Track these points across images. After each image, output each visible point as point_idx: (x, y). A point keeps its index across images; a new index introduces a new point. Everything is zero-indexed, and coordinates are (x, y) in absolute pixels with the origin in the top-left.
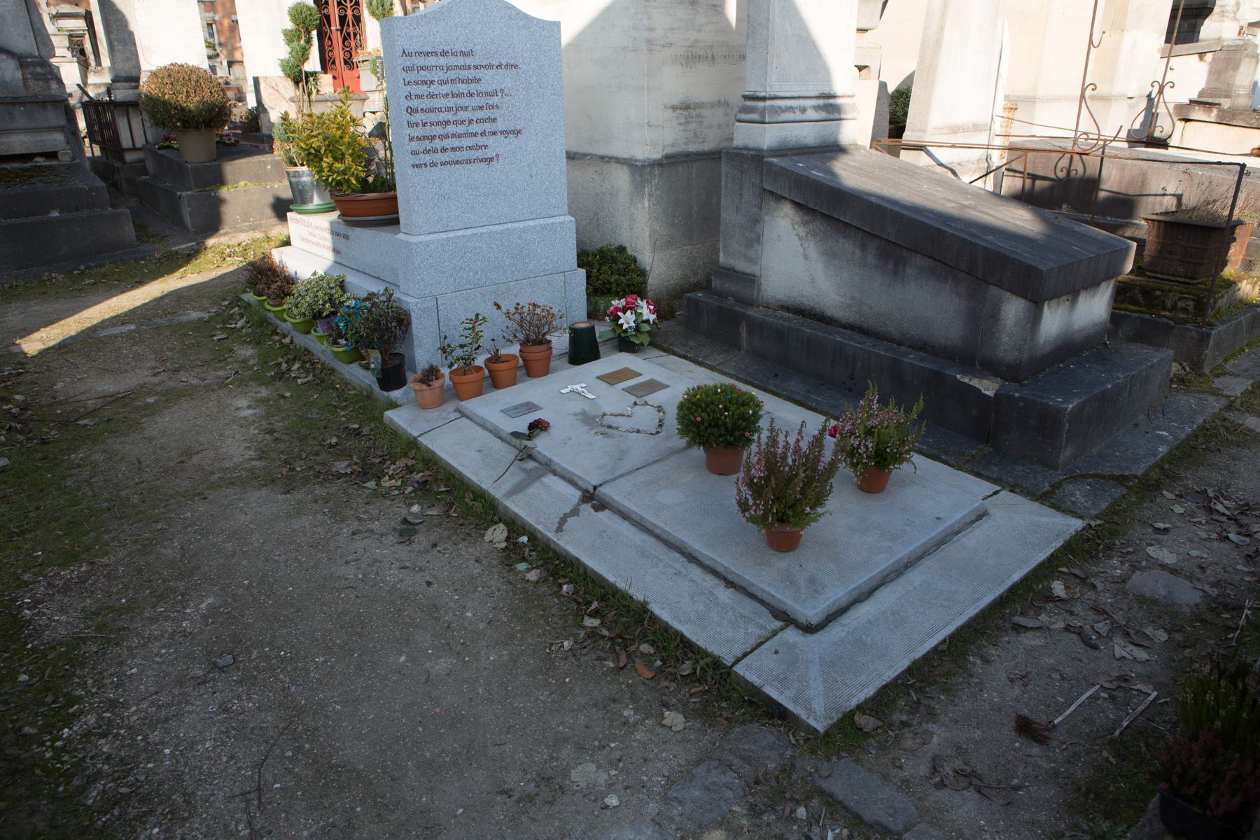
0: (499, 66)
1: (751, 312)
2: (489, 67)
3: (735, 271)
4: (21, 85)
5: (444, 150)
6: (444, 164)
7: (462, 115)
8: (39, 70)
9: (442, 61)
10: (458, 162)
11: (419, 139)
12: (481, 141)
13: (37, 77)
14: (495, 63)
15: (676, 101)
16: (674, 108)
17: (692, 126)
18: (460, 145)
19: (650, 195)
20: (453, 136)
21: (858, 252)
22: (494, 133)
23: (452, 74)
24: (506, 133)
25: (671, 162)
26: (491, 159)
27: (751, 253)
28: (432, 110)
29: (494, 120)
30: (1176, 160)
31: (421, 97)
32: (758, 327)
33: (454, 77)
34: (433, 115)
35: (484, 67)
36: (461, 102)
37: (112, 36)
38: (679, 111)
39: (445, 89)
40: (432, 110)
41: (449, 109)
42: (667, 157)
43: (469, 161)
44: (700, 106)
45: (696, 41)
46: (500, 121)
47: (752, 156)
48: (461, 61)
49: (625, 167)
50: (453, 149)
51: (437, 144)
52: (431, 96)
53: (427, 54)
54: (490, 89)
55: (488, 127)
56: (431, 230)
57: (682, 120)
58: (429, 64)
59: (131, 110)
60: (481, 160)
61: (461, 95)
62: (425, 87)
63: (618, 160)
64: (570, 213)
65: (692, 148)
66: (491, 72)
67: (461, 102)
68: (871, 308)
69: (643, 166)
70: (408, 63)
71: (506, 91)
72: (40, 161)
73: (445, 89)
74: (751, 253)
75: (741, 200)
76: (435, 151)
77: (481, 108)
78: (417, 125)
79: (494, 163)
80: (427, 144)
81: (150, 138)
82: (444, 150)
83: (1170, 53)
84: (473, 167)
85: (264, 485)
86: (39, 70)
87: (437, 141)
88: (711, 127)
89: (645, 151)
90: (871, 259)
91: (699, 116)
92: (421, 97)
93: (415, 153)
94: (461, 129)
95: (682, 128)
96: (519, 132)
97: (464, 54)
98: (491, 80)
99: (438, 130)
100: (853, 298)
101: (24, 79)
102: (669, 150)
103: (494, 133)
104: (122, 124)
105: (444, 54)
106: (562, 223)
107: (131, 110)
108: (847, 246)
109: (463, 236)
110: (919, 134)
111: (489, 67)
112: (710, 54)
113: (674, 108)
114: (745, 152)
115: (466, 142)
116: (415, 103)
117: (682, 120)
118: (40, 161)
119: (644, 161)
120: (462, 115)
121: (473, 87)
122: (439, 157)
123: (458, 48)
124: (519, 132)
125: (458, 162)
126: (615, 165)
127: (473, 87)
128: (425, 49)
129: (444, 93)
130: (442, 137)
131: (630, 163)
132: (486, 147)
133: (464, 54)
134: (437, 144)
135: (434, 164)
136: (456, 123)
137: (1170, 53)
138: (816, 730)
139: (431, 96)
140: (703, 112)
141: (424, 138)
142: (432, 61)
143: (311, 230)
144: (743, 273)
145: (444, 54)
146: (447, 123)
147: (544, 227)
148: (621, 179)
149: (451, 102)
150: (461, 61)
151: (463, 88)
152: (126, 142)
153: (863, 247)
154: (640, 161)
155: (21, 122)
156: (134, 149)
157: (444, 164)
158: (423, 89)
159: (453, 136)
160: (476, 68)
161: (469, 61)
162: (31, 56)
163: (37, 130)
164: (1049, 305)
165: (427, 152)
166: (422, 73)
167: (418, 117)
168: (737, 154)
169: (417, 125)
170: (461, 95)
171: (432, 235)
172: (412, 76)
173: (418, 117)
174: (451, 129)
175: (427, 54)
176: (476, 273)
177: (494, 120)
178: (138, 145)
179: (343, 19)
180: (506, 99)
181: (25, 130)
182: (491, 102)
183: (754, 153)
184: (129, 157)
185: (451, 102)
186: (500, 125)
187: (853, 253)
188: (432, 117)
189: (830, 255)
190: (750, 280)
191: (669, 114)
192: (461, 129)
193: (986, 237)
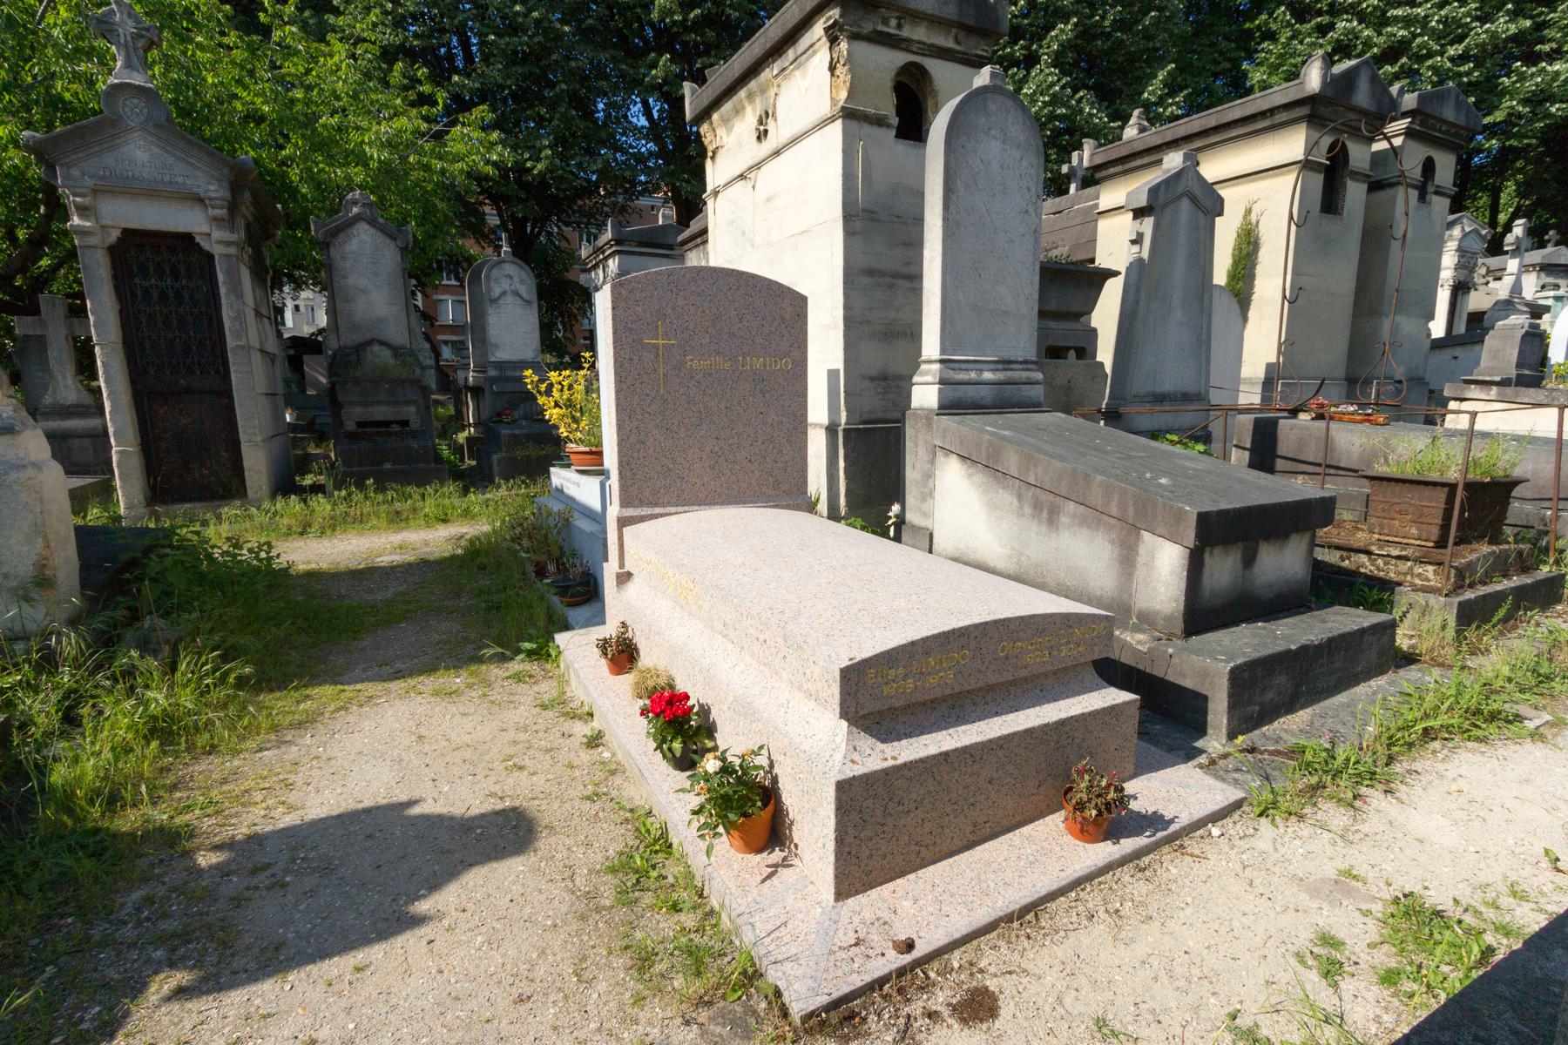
21: (1015, 502)
27: (925, 507)
57: (881, 390)
68: (1029, 558)
74: (925, 507)
83: (1321, 384)
85: (1315, 789)
90: (1028, 510)
91: (898, 387)
100: (1013, 549)
108: (1007, 498)
112: (908, 331)
113: (872, 379)
117: (881, 390)
118: (396, 428)
137: (1321, 384)
138: (1395, 641)
153: (1020, 497)
162: (404, 348)
164: (1211, 554)
189: (993, 506)
193: (1108, 368)
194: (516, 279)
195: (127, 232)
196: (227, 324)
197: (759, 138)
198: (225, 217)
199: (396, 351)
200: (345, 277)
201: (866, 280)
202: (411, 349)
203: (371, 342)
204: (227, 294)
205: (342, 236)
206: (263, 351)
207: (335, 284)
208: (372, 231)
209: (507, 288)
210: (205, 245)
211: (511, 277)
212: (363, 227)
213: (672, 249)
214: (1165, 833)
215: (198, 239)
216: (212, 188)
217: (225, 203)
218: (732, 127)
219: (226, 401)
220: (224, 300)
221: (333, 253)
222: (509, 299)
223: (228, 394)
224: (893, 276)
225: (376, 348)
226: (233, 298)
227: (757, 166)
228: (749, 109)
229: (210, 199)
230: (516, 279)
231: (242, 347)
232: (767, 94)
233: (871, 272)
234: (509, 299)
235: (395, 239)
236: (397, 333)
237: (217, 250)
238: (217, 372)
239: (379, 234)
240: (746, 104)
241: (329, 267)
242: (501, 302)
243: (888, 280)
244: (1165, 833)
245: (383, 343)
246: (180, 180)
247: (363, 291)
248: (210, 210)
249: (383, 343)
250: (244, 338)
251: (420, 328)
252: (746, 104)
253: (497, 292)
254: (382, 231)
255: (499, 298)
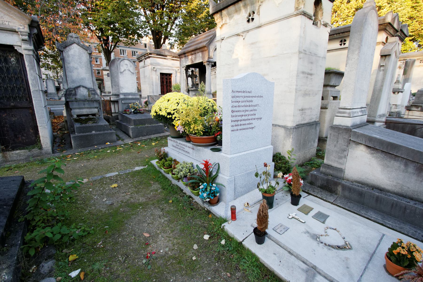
0: (258, 97)
1: (343, 182)
2: (255, 97)
3: (332, 166)
4: (88, 95)
5: (241, 125)
6: (240, 130)
7: (247, 113)
8: (93, 92)
9: (243, 94)
10: (244, 129)
11: (234, 121)
12: (251, 121)
13: (92, 94)
14: (257, 95)
15: (300, 108)
16: (300, 110)
17: (303, 116)
18: (245, 123)
19: (292, 138)
20: (244, 120)
22: (255, 119)
23: (245, 99)
24: (258, 119)
25: (298, 127)
26: (253, 128)
28: (239, 111)
29: (255, 115)
30: (400, 122)
31: (236, 107)
32: (344, 187)
33: (246, 100)
34: (239, 113)
35: (254, 97)
36: (247, 108)
37: (113, 84)
38: (301, 111)
39: (243, 104)
40: (239, 111)
41: (243, 111)
42: (297, 125)
43: (247, 129)
44: (305, 109)
45: (307, 89)
46: (256, 115)
47: (344, 128)
48: (248, 94)
49: (282, 128)
50: (243, 125)
51: (239, 123)
52: (239, 106)
53: (239, 92)
54: (255, 104)
55: (253, 117)
56: (235, 153)
58: (239, 95)
59: (115, 103)
60: (250, 128)
61: (247, 106)
62: (238, 103)
63: (279, 126)
64: (272, 145)
65: (303, 122)
66: (256, 98)
67: (247, 108)
69: (291, 129)
70: (233, 95)
71: (259, 105)
72: (91, 117)
73: (243, 104)
75: (337, 143)
76: (238, 125)
77: (252, 110)
78: (234, 116)
79: (254, 129)
80: (236, 123)
81: (120, 110)
82: (241, 125)
84: (248, 130)
86: (93, 92)
87: (239, 122)
88: (307, 116)
89: (290, 124)
92: (236, 107)
93: (232, 126)
94: (246, 118)
95: (301, 116)
96: (261, 118)
97: (249, 92)
98: (256, 101)
99: (240, 118)
101: (89, 94)
102: (298, 123)
103: (255, 119)
104: (112, 106)
105: (244, 92)
106: (270, 148)
107: (115, 103)
109: (244, 154)
110: (373, 118)
111: (255, 97)
113: (300, 110)
114: (339, 127)
115: (247, 122)
116: (234, 109)
119: (291, 127)
120: (247, 113)
121: (251, 104)
122: (239, 127)
123: (248, 90)
124: (261, 118)
125: (244, 129)
126: (278, 127)
127: (251, 104)
128: (238, 90)
129: (242, 105)
130: (241, 120)
131: (285, 127)
132: (252, 123)
133: (249, 92)
134: (239, 123)
135: (237, 130)
136: (245, 116)
139: (239, 106)
140: (306, 111)
141: (236, 121)
142: (240, 94)
143: (177, 144)
144: (336, 167)
145: (244, 92)
146: (242, 116)
147: (265, 150)
148: (281, 132)
149: (244, 108)
150: (248, 94)
151: (248, 104)
152: (113, 111)
153: (406, 165)
154: (289, 127)
155: (86, 106)
156: (115, 113)
157: (240, 130)
158: (237, 104)
159: (244, 120)
160: (252, 97)
161: (250, 95)
162: (91, 88)
163: (91, 108)
165: (236, 126)
166: (237, 98)
167: (235, 114)
168: (337, 128)
169: (234, 116)
170: (247, 106)
171: (236, 154)
172: (234, 99)
173: (235, 114)
174: (243, 118)
175: (239, 92)
176: (246, 167)
177: (255, 115)
178: (116, 112)
179: (167, 82)
180: (259, 107)
181: (88, 108)
182: (255, 109)
183: (345, 127)
184: (113, 115)
185: (244, 108)
186: (256, 116)
187: (400, 167)
188: (238, 114)
190: (341, 170)
191: (299, 112)
192: (246, 118)
194: (129, 65)
195: (186, 66)
196: (30, 82)
197: (248, 21)
198: (27, 39)
199: (88, 89)
200: (69, 63)
201: (302, 75)
202: (94, 89)
203: (79, 87)
204: (30, 70)
205: (68, 48)
206: (42, 91)
207: (66, 66)
208: (79, 47)
209: (126, 68)
210: (20, 51)
211: (127, 65)
212: (75, 45)
213: (166, 57)
214: (110, 131)
215: (16, 48)
216: (21, 27)
217: (27, 34)
218: (233, 17)
219: (31, 111)
220: (28, 72)
221: (64, 54)
222: (127, 72)
223: (32, 108)
224: (308, 74)
225: (82, 89)
226: (32, 72)
227: (248, 31)
228: (243, 10)
229: (21, 32)
230: (129, 65)
231: (37, 91)
232: (255, 5)
233: (303, 73)
234: (127, 72)
235: (87, 50)
236: (89, 84)
237: (24, 53)
238: (27, 100)
239: (81, 48)
240: (242, 8)
241: (63, 59)
242: (124, 73)
243: (307, 75)
244: (110, 131)
245: (83, 87)
246: (7, 23)
247: (77, 69)
248: (21, 36)
249: (83, 87)
250: (38, 88)
251: (96, 83)
252: (242, 8)
253: (122, 70)
254: (82, 47)
255: (123, 71)
